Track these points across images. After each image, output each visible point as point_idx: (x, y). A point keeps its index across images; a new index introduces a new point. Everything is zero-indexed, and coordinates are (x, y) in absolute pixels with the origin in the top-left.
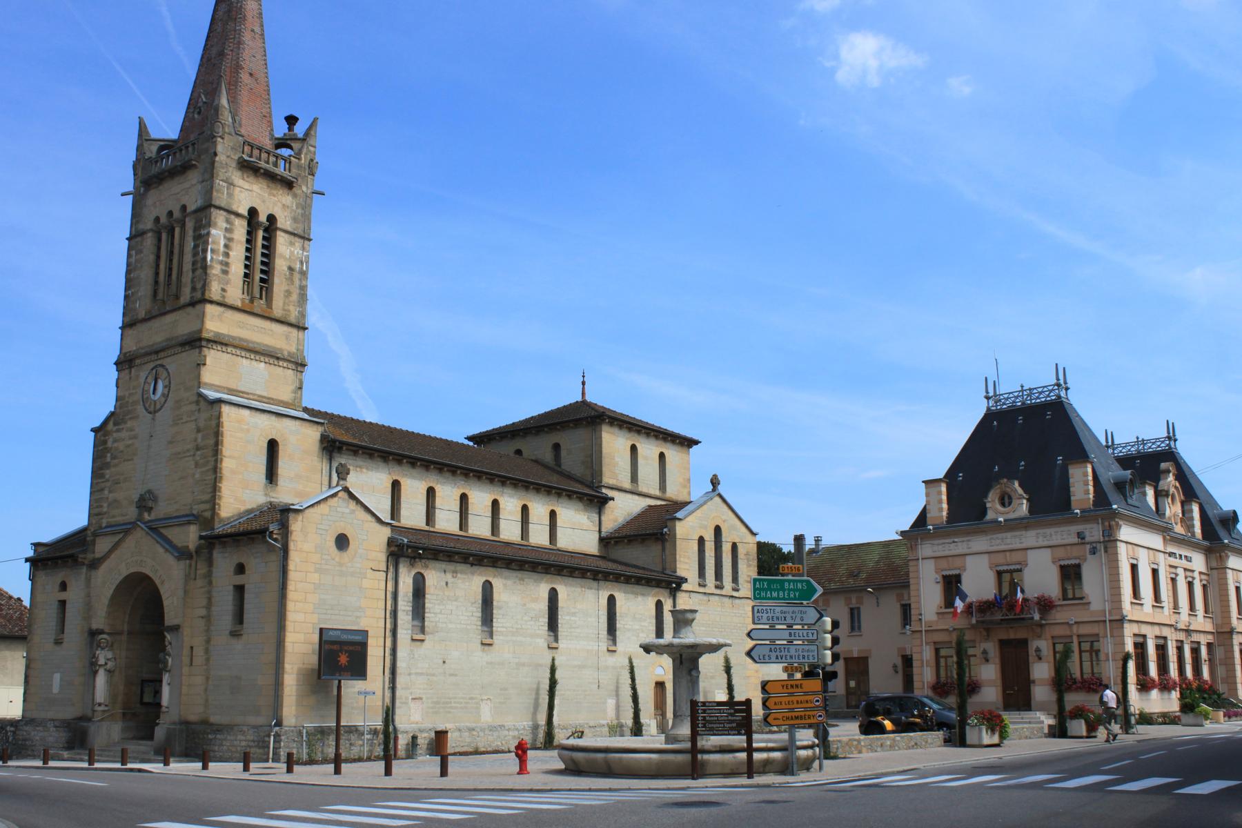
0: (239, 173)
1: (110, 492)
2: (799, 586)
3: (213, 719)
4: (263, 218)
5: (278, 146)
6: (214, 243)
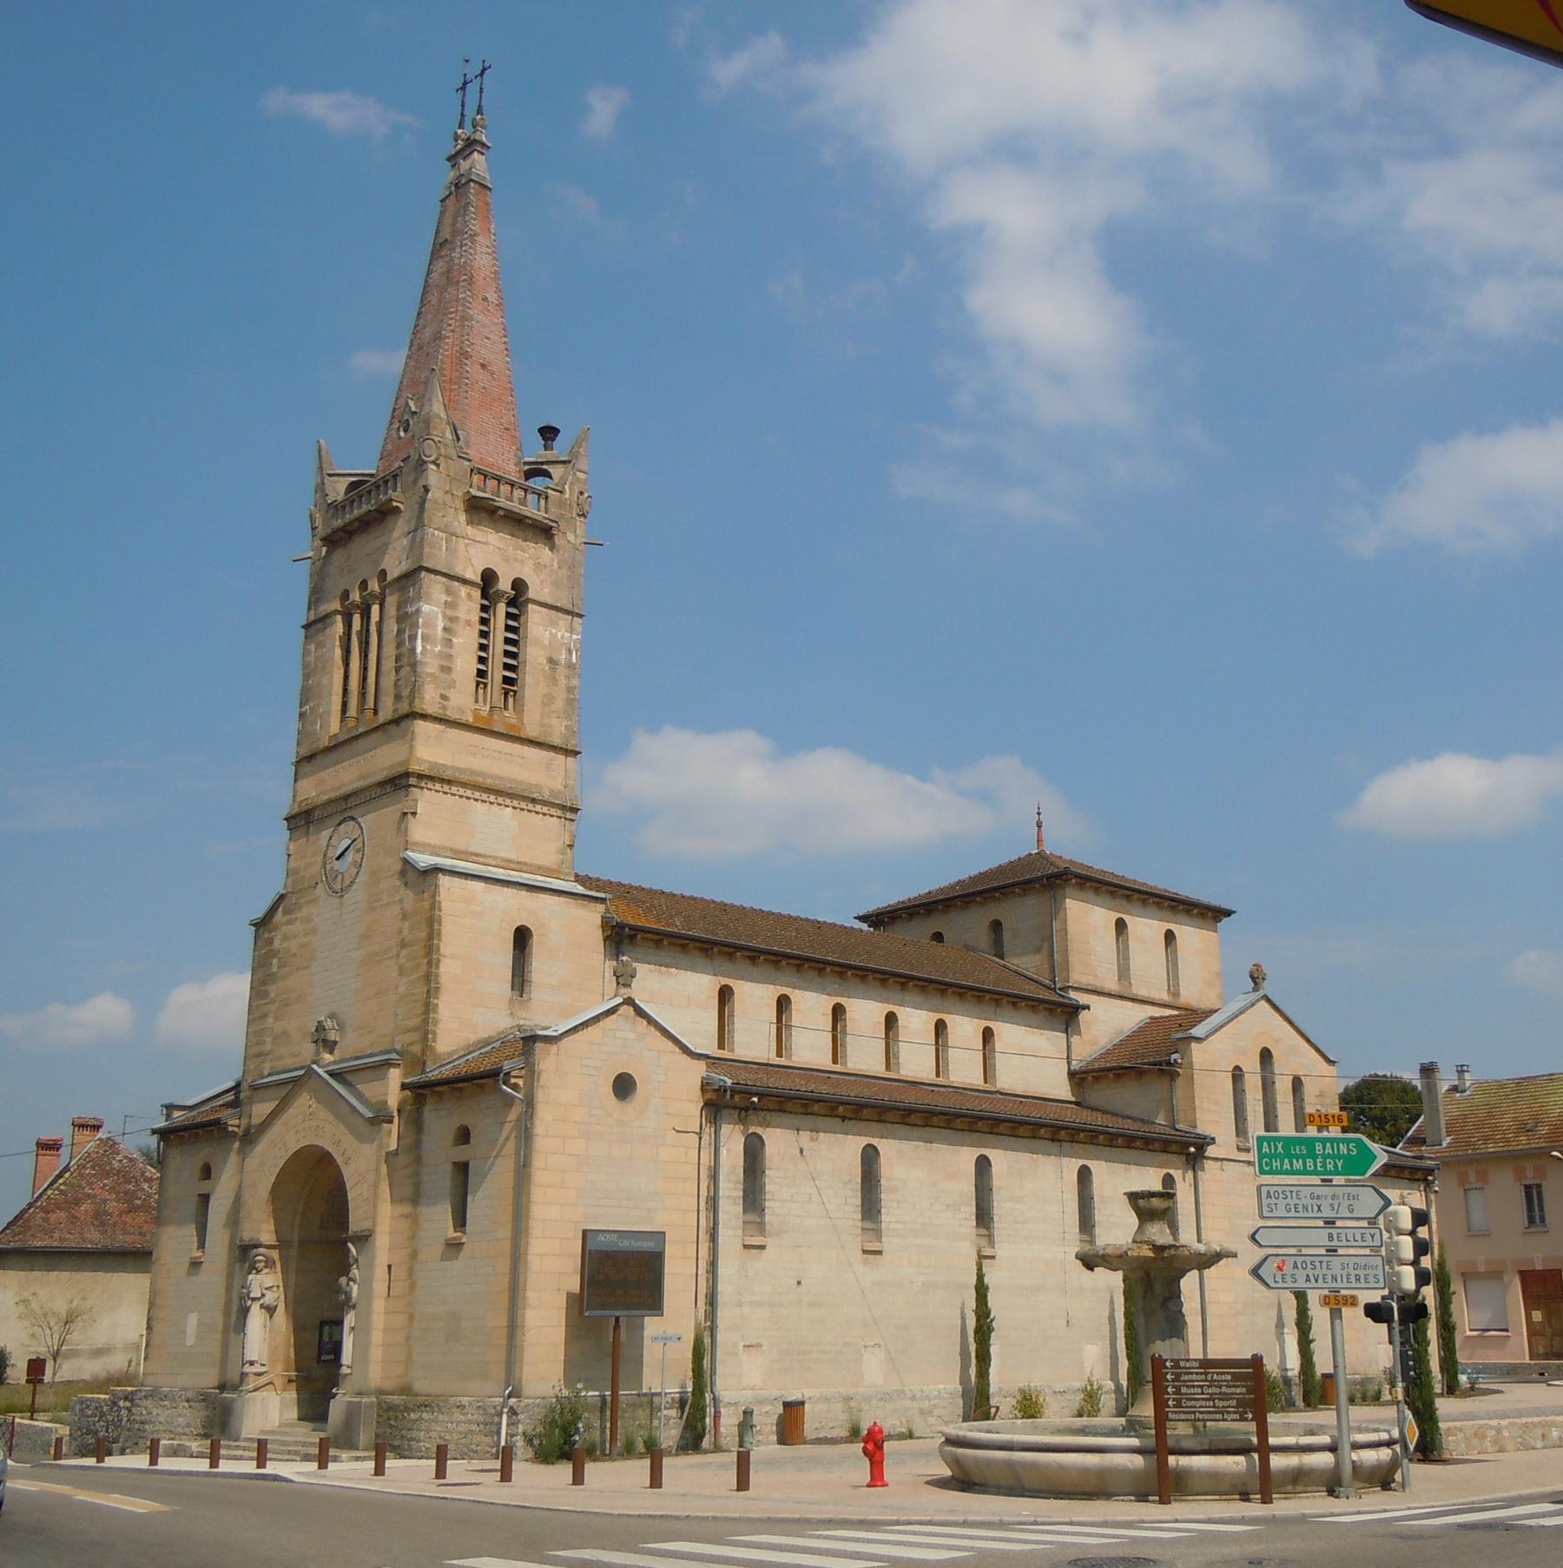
0: (470, 522)
1: (276, 1019)
2: (1343, 1149)
3: (420, 1386)
4: (504, 585)
5: (529, 475)
6: (426, 625)
